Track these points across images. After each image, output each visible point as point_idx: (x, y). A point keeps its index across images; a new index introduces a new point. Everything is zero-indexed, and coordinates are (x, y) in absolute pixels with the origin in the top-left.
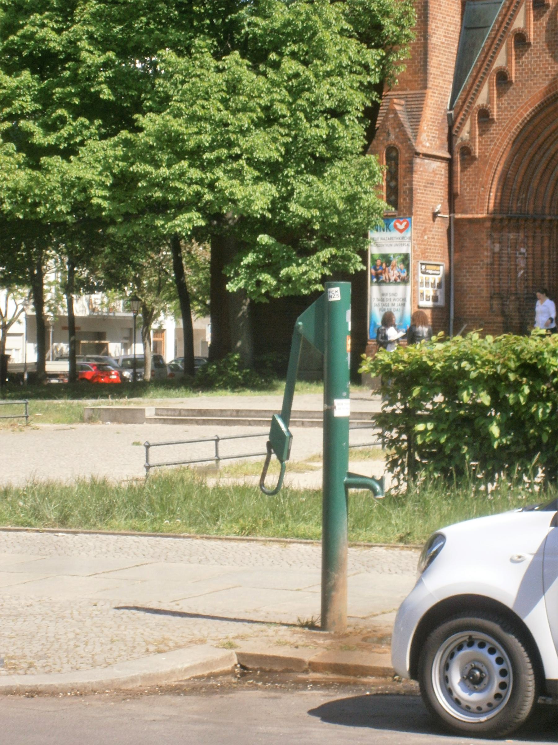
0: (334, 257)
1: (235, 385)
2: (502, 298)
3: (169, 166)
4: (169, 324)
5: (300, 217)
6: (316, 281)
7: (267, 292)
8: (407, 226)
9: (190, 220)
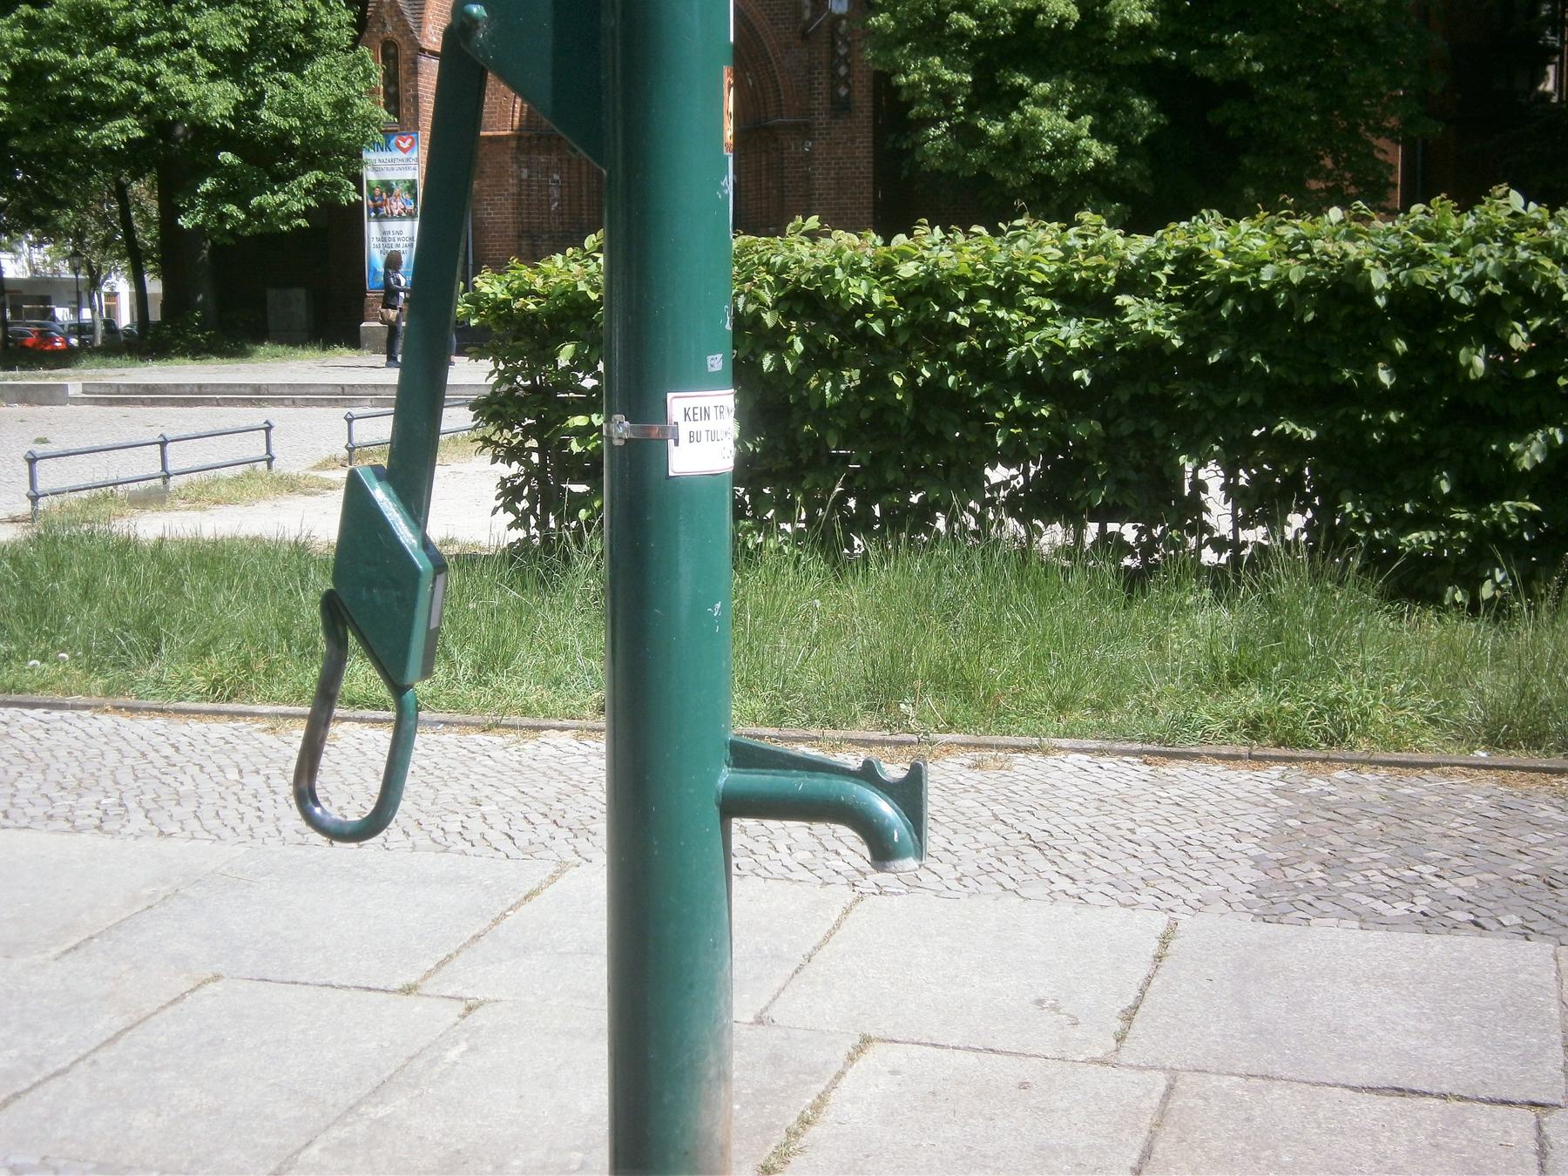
0: (320, 183)
1: (198, 351)
2: (532, 237)
3: (90, 55)
4: (122, 286)
5: (273, 127)
6: (297, 215)
7: (233, 228)
8: (412, 145)
9: (122, 130)
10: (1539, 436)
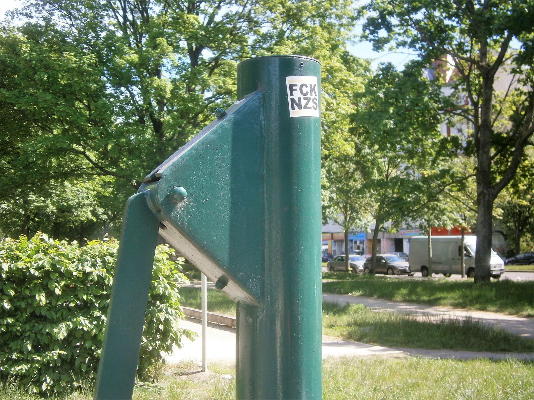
10: (64, 326)
